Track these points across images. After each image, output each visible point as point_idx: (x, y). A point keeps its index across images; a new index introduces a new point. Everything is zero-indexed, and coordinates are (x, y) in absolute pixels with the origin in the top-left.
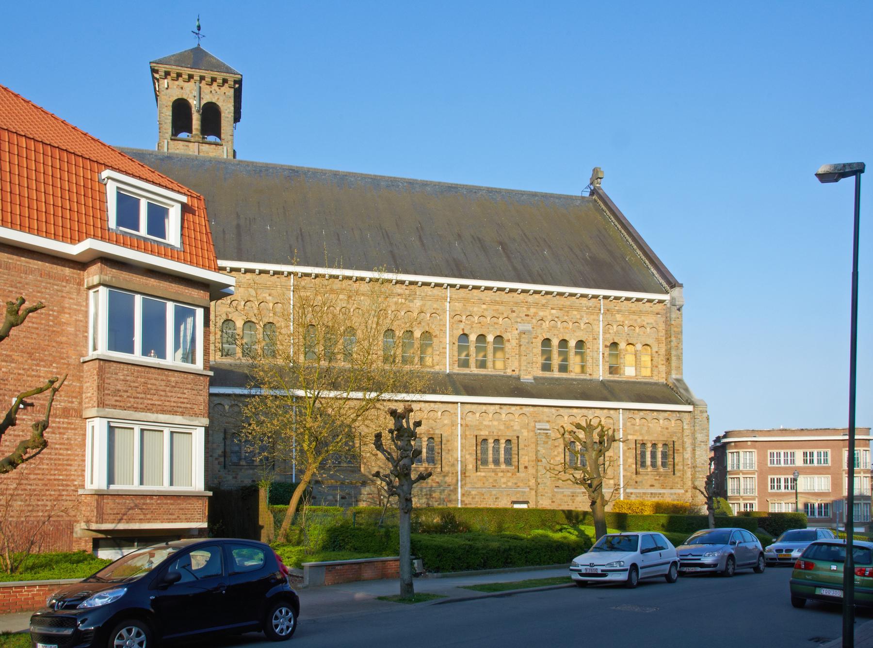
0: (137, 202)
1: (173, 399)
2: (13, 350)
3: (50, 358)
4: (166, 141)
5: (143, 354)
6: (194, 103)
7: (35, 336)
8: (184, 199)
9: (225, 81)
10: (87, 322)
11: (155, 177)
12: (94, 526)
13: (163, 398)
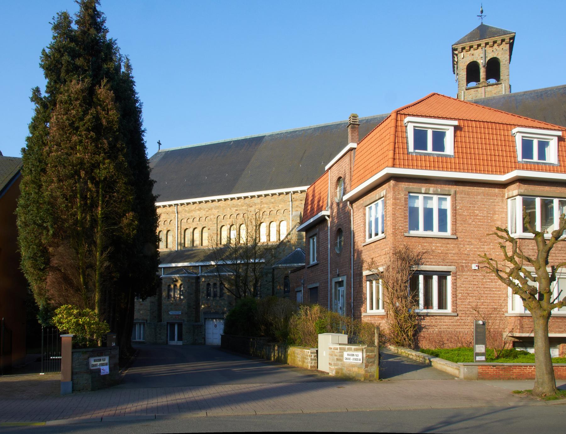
0: (426, 132)
1: (560, 258)
2: (472, 238)
3: (489, 241)
4: (463, 92)
5: (524, 232)
6: (481, 62)
7: (482, 229)
8: (560, 133)
9: (503, 41)
10: (507, 218)
11: (542, 125)
12: (518, 335)
13: (554, 258)
